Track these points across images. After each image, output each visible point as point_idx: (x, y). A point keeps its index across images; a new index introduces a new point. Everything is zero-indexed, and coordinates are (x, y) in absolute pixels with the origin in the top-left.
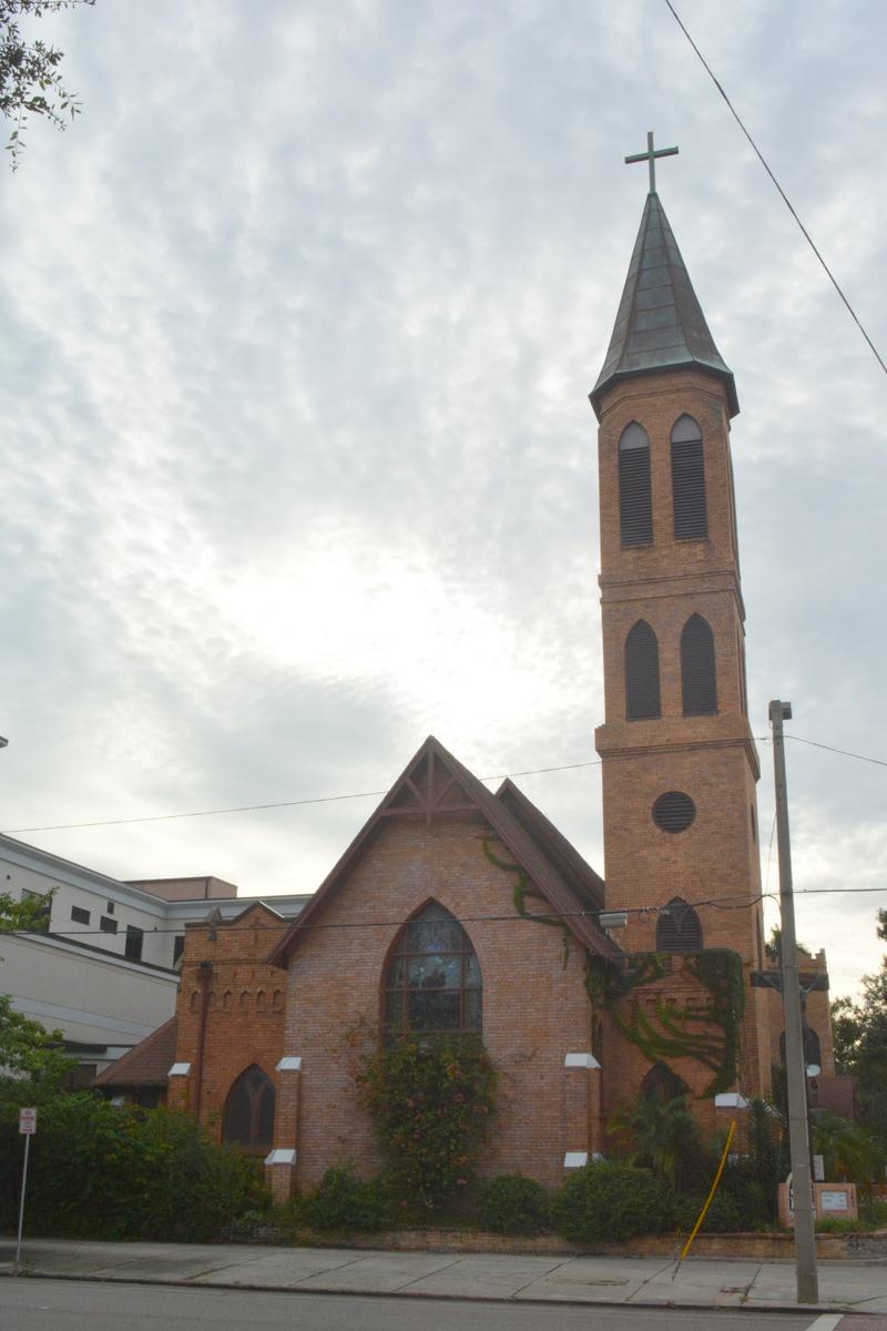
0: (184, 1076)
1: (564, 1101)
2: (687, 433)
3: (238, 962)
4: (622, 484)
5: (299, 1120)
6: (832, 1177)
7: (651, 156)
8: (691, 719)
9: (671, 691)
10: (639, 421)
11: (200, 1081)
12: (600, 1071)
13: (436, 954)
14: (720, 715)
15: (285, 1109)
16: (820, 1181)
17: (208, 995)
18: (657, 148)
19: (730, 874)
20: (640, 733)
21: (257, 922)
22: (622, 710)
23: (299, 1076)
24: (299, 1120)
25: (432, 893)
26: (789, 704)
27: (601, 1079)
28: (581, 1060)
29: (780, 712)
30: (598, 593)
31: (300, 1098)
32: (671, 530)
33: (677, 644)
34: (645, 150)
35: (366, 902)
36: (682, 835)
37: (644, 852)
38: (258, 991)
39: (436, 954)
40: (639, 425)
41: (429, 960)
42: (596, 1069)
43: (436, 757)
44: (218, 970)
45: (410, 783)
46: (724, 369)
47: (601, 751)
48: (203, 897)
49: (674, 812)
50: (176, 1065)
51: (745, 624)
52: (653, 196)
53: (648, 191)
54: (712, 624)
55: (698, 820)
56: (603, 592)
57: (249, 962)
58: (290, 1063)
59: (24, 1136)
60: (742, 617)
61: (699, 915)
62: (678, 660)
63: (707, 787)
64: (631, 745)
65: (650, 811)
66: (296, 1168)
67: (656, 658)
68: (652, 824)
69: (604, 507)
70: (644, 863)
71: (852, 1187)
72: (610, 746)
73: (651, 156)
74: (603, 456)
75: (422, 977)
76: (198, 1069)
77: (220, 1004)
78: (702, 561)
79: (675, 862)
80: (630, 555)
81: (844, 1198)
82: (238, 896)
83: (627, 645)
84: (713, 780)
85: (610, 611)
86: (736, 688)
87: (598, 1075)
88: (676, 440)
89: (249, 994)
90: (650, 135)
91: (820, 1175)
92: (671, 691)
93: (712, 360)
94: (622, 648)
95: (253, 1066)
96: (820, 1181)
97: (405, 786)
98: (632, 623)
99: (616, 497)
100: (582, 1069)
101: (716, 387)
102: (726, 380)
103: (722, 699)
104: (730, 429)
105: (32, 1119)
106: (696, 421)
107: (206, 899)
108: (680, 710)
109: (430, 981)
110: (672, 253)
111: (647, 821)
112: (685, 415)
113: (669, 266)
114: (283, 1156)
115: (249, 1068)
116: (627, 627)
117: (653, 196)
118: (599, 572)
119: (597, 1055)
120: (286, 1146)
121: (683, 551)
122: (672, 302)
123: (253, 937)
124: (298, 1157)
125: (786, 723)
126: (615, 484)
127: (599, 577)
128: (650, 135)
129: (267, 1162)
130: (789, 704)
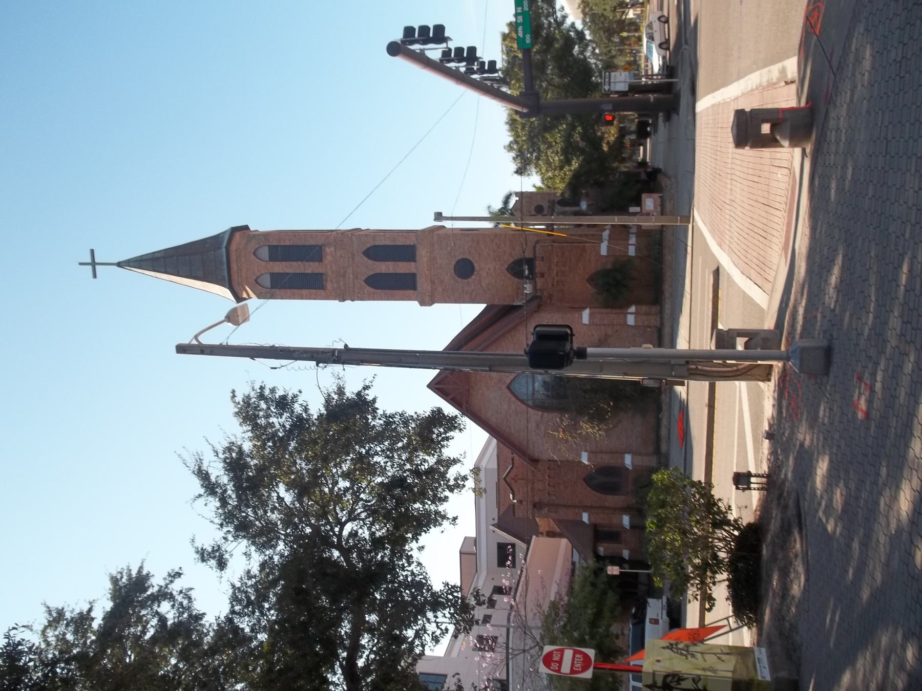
0: (589, 516)
1: (604, 325)
2: (265, 253)
3: (533, 489)
4: (290, 288)
5: (611, 452)
6: (638, 203)
7: (93, 264)
8: (418, 258)
9: (402, 267)
10: (255, 277)
11: (592, 507)
12: (591, 308)
13: (533, 385)
14: (416, 244)
15: (606, 460)
16: (641, 209)
17: (549, 505)
18: (89, 261)
19: (496, 243)
20: (423, 283)
21: (512, 479)
22: (411, 292)
23: (592, 453)
24: (611, 452)
25: (504, 387)
26: (435, 213)
27: (595, 308)
28: (586, 315)
29: (439, 216)
30: (348, 302)
31: (601, 452)
32: (317, 264)
33: (378, 263)
34: (90, 267)
35: (507, 420)
36: (476, 265)
37: (483, 284)
38: (547, 477)
39: (533, 385)
40: (257, 277)
41: (536, 389)
42: (590, 310)
43: (437, 384)
44: (537, 500)
45: (450, 397)
46: (229, 231)
47: (431, 304)
48: (474, 556)
49: (465, 269)
50: (584, 520)
51: (363, 228)
52: (119, 265)
53: (115, 267)
54: (368, 246)
55: (468, 257)
56: (348, 300)
57: (533, 483)
58: (585, 460)
59: (620, 572)
60: (369, 229)
61: (516, 258)
62: (387, 263)
63: (452, 252)
64: (429, 288)
65: (463, 280)
66: (634, 453)
67: (385, 274)
68: (470, 280)
69: (302, 297)
70: (489, 285)
71: (644, 196)
72: (427, 301)
73: (93, 264)
74: (272, 297)
75: (545, 393)
76: (586, 508)
77: (554, 498)
78: (335, 249)
79: (489, 269)
80: (329, 286)
81: (648, 199)
82: (474, 536)
83: (377, 288)
84: (449, 249)
85: (358, 297)
86: (403, 235)
87: (592, 309)
88: (267, 258)
89: (549, 483)
90: (81, 264)
91: (637, 209)
92: (402, 267)
93: (223, 237)
94: (379, 291)
95: (585, 480)
96: (641, 209)
97: (451, 399)
98: (366, 285)
99: (296, 291)
100: (591, 315)
101: (237, 235)
102: (234, 230)
103: (408, 243)
104: (257, 231)
105: (612, 569)
106: (258, 248)
107: (476, 554)
108: (413, 263)
109: (547, 389)
110: (156, 255)
111: (468, 283)
112: (254, 254)
113: (165, 258)
114: (628, 460)
115: (585, 482)
116: (368, 289)
117: (119, 265)
118: (337, 301)
119: (585, 308)
120: (623, 459)
121: (329, 258)
122: (188, 257)
123: (521, 481)
124: (629, 453)
125: (443, 215)
126: (289, 291)
127: (340, 301)
128: (81, 264)
129: (630, 468)
130: (435, 213)
